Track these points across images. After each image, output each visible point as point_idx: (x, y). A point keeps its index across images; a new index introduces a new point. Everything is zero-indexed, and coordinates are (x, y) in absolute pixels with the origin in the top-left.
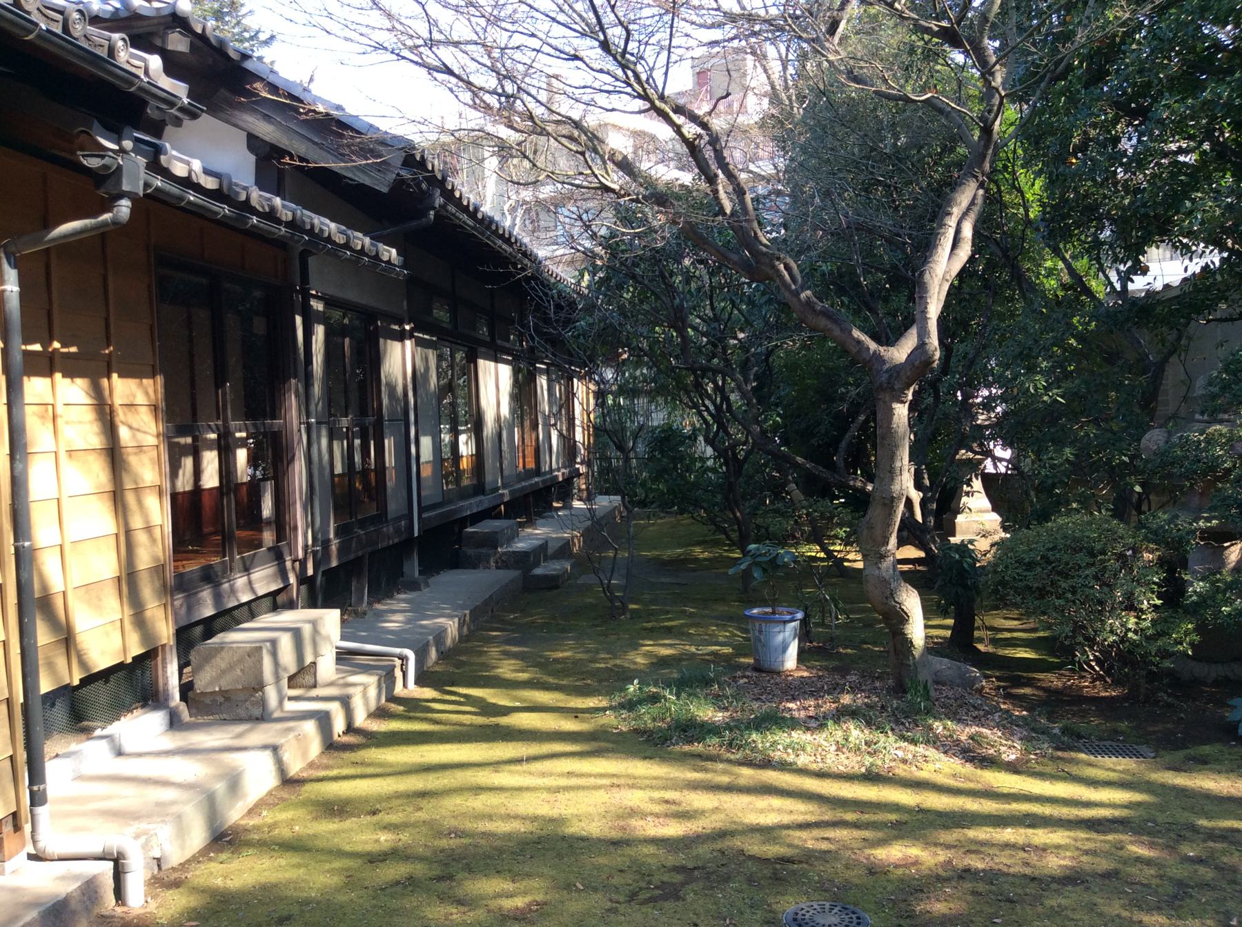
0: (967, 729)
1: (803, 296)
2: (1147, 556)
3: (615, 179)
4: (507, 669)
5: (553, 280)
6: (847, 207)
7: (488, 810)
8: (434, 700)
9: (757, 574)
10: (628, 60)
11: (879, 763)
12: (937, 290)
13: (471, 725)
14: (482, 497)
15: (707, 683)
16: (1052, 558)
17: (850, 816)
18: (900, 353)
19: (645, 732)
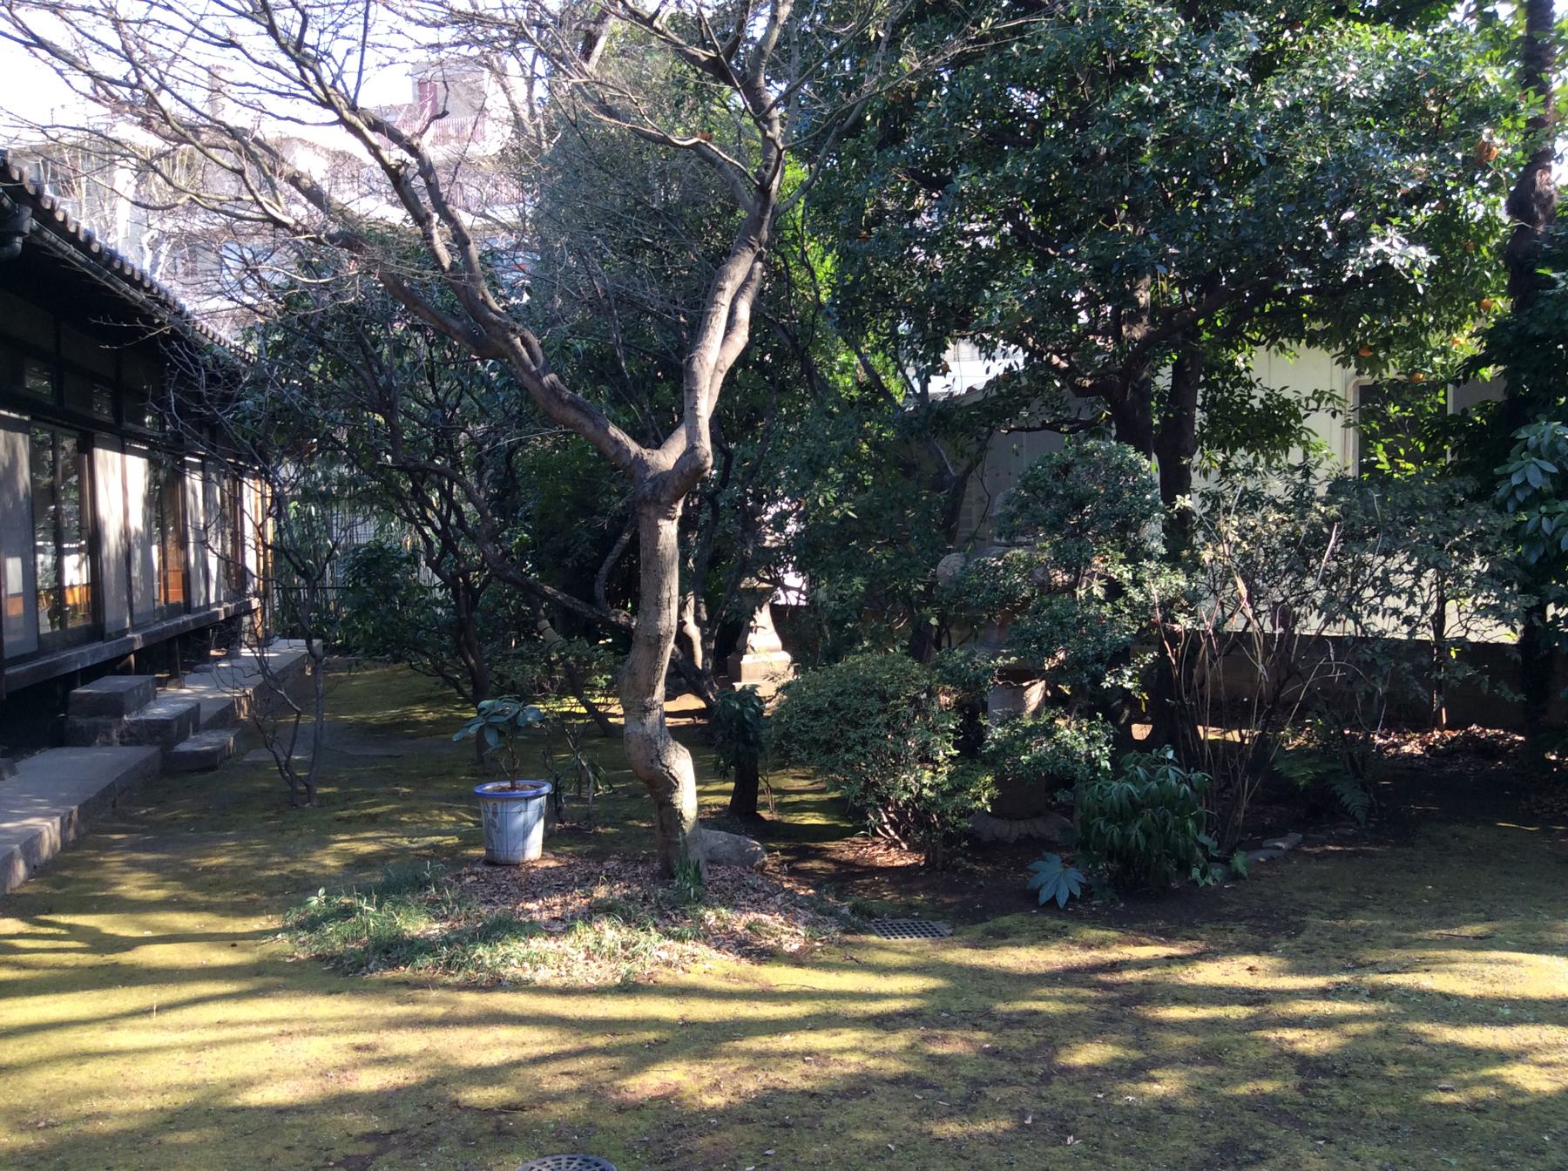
0: (744, 917)
1: (546, 380)
2: (944, 699)
3: (298, 211)
4: (133, 886)
5: (208, 342)
6: (607, 271)
7: (96, 1084)
8: (21, 936)
9: (491, 739)
10: (307, 56)
11: (638, 969)
12: (708, 382)
13: (76, 967)
14: (99, 645)
15: (422, 885)
16: (841, 705)
17: (599, 1041)
18: (667, 457)
19: (332, 958)
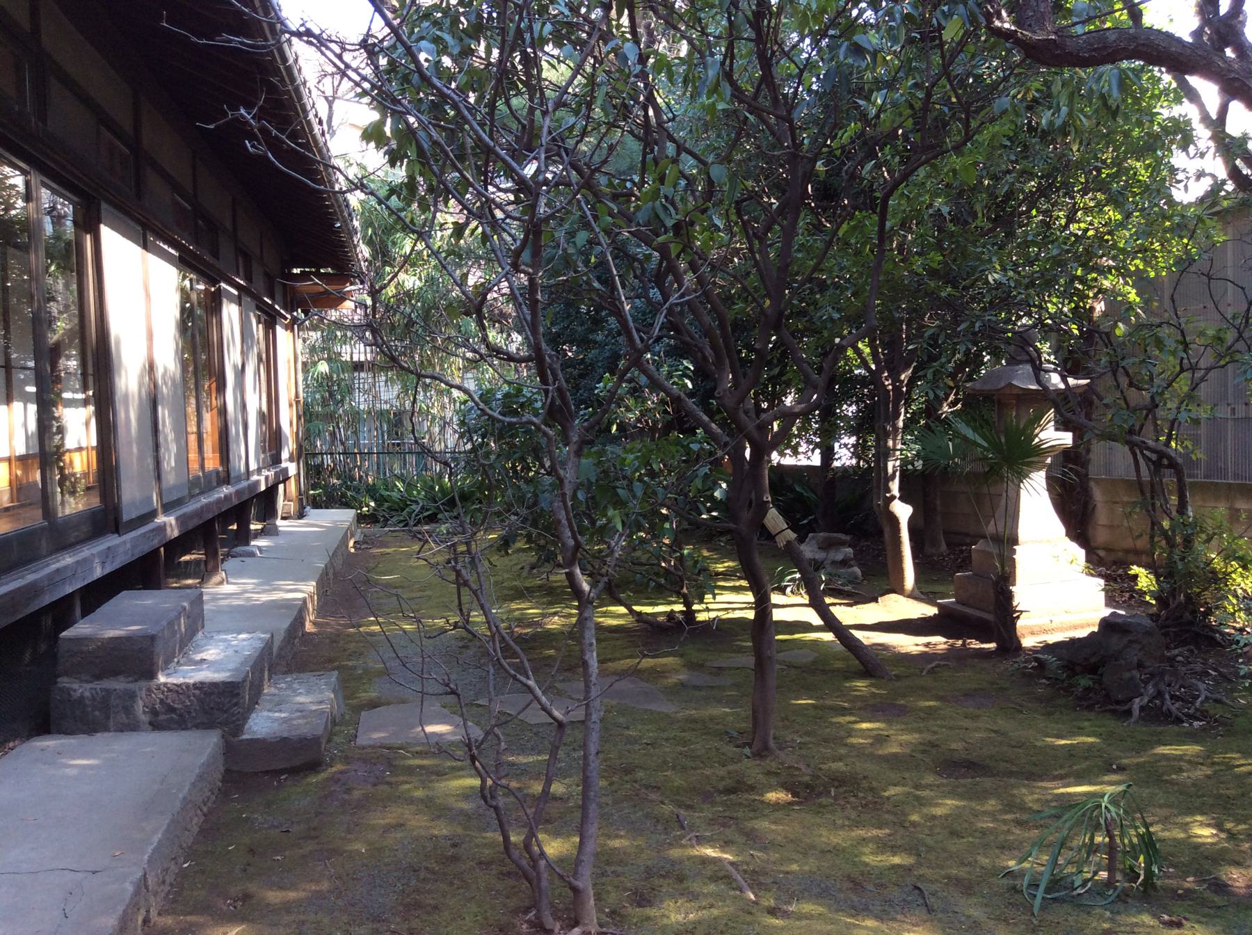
14: (112, 541)
